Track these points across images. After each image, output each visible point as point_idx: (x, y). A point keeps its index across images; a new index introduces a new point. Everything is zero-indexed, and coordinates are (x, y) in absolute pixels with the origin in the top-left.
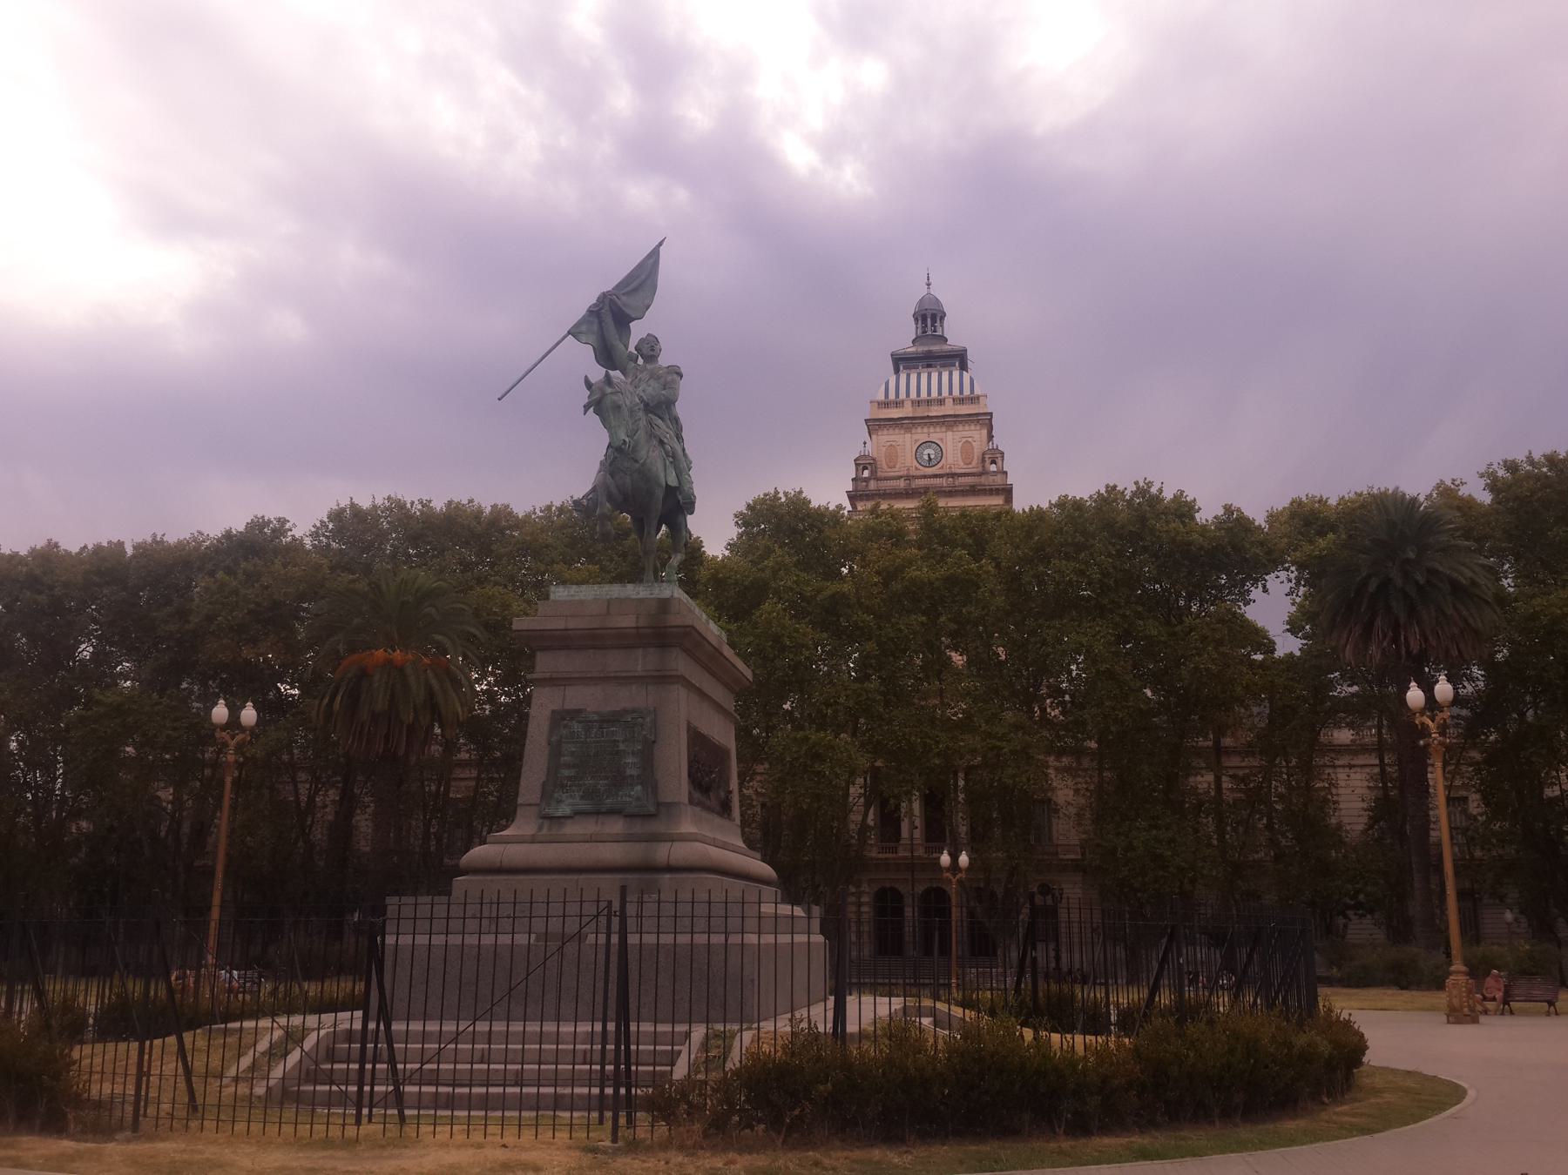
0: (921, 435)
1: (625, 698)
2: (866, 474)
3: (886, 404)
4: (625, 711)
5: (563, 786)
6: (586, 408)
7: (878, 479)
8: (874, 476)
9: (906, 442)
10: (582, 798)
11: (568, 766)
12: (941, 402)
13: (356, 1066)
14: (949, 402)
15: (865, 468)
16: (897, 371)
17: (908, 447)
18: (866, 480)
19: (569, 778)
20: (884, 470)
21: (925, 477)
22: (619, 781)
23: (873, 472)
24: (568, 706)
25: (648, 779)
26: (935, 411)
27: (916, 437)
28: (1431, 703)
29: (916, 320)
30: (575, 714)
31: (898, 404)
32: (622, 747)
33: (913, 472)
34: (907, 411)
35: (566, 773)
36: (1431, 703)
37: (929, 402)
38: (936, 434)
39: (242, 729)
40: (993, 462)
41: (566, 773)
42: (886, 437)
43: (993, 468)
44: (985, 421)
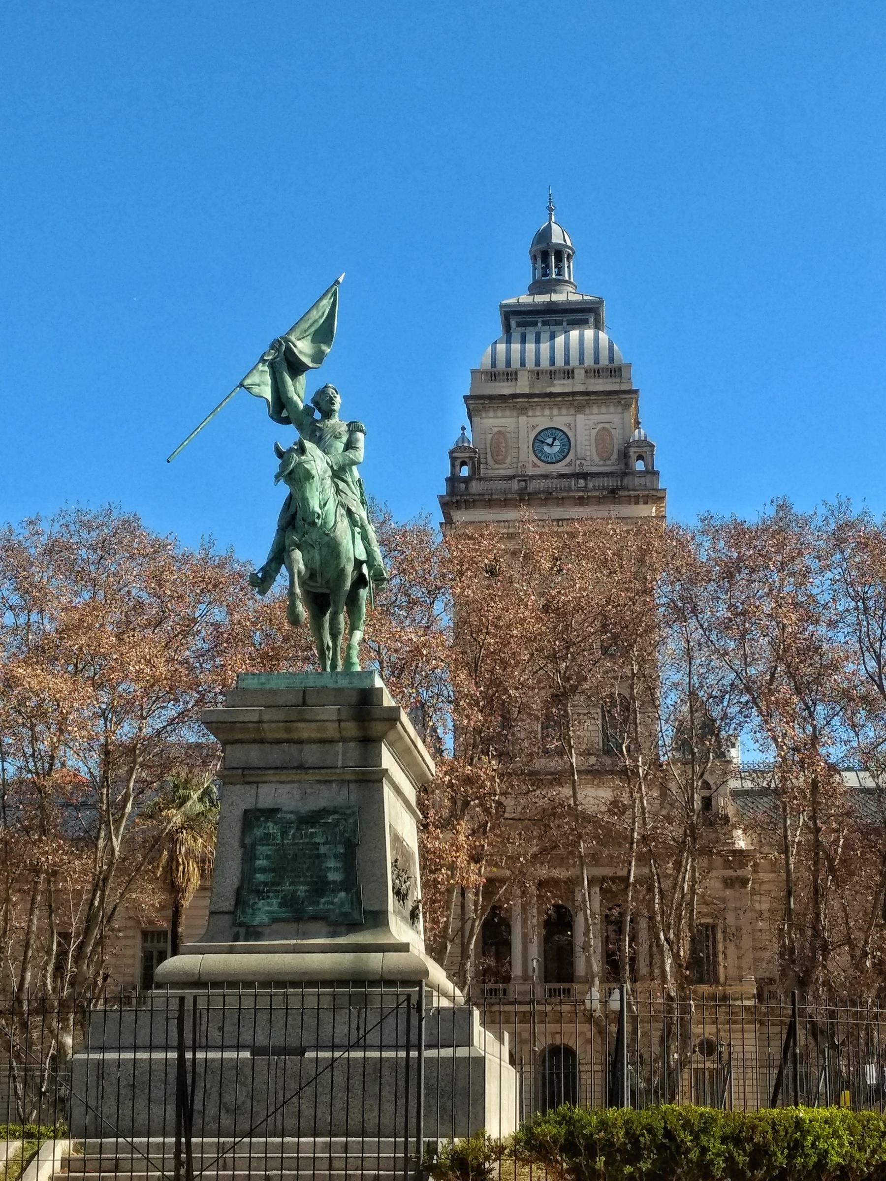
0: (542, 419)
2: (465, 471)
3: (493, 375)
4: (324, 812)
5: (259, 893)
6: (277, 477)
7: (481, 479)
8: (475, 473)
9: (524, 427)
10: (280, 905)
11: (263, 870)
12: (569, 374)
13: (174, 1140)
14: (580, 374)
15: (464, 463)
16: (507, 329)
17: (523, 433)
18: (467, 480)
19: (266, 884)
20: (492, 469)
21: (545, 476)
22: (320, 888)
23: (475, 470)
24: (261, 805)
26: (560, 386)
27: (533, 421)
29: (534, 258)
30: (271, 813)
31: (511, 376)
32: (323, 850)
33: (530, 471)
34: (523, 386)
35: (260, 877)
37: (552, 374)
38: (560, 419)
40: (640, 458)
41: (260, 877)
42: (495, 421)
43: (640, 466)
44: (624, 398)
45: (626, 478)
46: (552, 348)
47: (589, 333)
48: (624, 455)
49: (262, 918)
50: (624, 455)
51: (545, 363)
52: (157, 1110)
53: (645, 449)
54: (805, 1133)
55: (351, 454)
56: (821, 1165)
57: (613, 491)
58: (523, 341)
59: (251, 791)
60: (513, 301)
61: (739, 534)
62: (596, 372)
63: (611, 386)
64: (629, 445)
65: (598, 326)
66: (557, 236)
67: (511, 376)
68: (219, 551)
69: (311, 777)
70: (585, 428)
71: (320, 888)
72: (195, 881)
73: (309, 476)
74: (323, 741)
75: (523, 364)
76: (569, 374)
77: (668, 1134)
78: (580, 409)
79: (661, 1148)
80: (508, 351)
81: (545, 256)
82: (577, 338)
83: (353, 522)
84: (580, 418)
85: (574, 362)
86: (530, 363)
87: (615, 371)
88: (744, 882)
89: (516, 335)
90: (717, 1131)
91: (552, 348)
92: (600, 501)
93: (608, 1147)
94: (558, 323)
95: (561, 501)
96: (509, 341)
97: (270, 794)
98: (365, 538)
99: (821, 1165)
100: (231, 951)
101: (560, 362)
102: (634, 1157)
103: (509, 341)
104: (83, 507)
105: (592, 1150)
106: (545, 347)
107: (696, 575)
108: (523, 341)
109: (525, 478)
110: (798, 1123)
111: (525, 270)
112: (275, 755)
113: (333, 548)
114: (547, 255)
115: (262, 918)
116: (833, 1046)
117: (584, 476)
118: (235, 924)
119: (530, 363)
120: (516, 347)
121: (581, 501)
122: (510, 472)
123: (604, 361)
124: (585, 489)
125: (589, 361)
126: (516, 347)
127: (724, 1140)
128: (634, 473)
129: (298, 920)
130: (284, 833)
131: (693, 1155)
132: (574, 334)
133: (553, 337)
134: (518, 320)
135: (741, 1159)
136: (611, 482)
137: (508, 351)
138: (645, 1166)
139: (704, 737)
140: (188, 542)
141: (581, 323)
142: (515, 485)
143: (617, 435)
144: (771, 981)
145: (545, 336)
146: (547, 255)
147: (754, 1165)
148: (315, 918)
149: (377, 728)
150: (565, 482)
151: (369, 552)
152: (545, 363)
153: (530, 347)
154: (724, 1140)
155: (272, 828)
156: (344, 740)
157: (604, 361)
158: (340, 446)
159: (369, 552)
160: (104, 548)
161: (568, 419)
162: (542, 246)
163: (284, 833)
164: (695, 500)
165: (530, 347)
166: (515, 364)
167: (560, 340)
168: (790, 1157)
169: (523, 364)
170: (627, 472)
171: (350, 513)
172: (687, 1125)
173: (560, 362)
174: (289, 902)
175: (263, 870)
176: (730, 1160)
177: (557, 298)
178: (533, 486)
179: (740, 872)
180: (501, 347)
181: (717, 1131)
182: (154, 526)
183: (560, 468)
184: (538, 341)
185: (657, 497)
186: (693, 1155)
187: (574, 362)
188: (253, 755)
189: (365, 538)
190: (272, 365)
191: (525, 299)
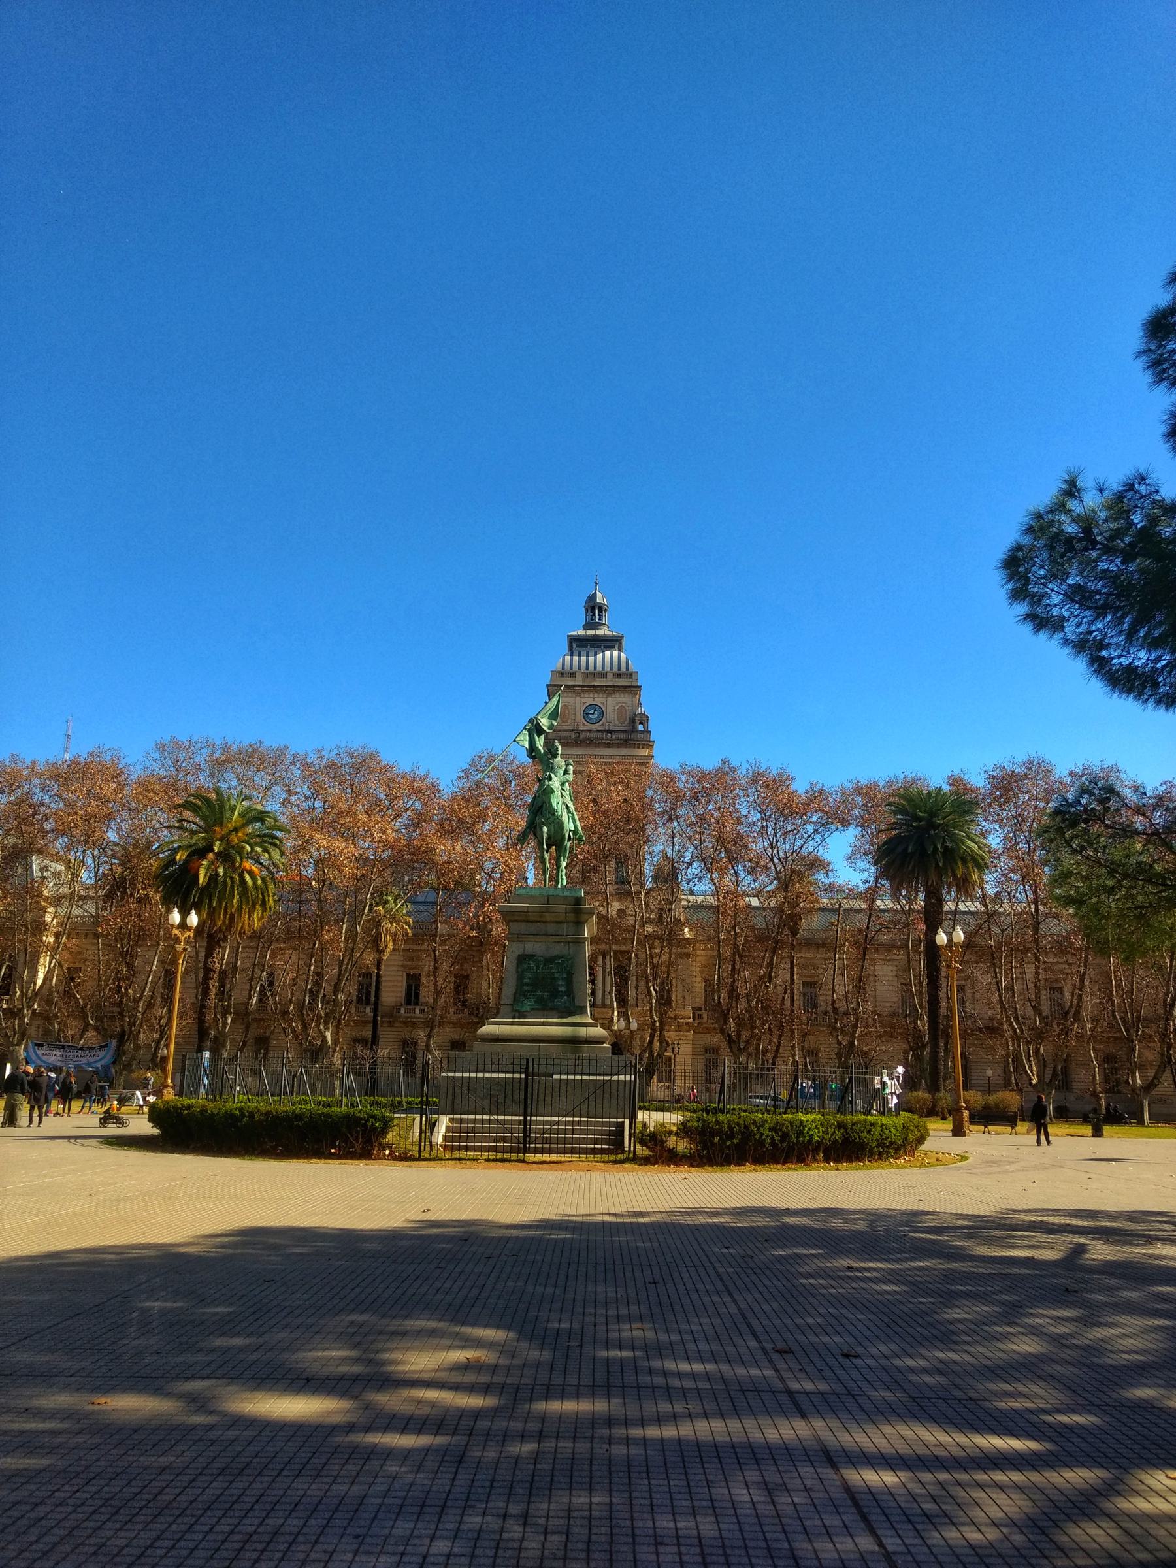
0: (588, 699)
1: (557, 950)
3: (563, 673)
4: (558, 957)
5: (525, 996)
11: (528, 984)
12: (604, 675)
14: (610, 676)
16: (571, 649)
22: (555, 994)
25: (570, 992)
27: (584, 700)
28: (183, 925)
29: (587, 610)
30: (531, 957)
31: (572, 674)
34: (579, 680)
35: (526, 988)
36: (183, 925)
38: (599, 700)
39: (189, 929)
41: (526, 988)
43: (641, 727)
44: (633, 690)
45: (632, 734)
46: (595, 660)
47: (615, 653)
48: (633, 721)
49: (526, 1008)
50: (633, 721)
51: (591, 668)
52: (480, 1103)
53: (644, 718)
54: (804, 1127)
55: (567, 777)
56: (810, 1141)
57: (626, 741)
58: (580, 655)
59: (521, 945)
60: (575, 633)
61: (703, 777)
62: (619, 675)
63: (626, 683)
64: (635, 716)
65: (620, 650)
66: (600, 599)
67: (572, 674)
68: (422, 772)
69: (551, 939)
70: (612, 705)
71: (555, 994)
72: (390, 945)
73: (553, 791)
74: (557, 922)
75: (579, 668)
76: (604, 675)
77: (746, 1127)
78: (609, 695)
79: (743, 1133)
80: (572, 660)
81: (593, 609)
82: (609, 656)
83: (569, 812)
84: (609, 699)
85: (607, 669)
86: (583, 668)
87: (630, 675)
88: (687, 955)
89: (576, 652)
90: (767, 1126)
91: (595, 660)
92: (619, 746)
93: (720, 1132)
94: (599, 647)
95: (597, 745)
96: (572, 655)
97: (532, 947)
98: (573, 819)
99: (810, 1141)
100: (512, 1024)
101: (599, 668)
102: (731, 1137)
103: (572, 655)
104: (349, 745)
105: (713, 1133)
106: (591, 659)
107: (679, 797)
108: (580, 655)
109: (578, 731)
110: (801, 1122)
111: (582, 617)
112: (532, 928)
113: (561, 825)
114: (593, 609)
115: (526, 1008)
116: (739, 1049)
117: (611, 732)
118: (513, 1010)
119: (583, 668)
120: (576, 658)
121: (609, 746)
122: (570, 728)
123: (623, 668)
124: (611, 739)
125: (615, 669)
126: (576, 658)
127: (770, 1130)
128: (638, 731)
129: (544, 1010)
130: (538, 967)
131: (757, 1137)
132: (608, 653)
133: (596, 655)
134: (577, 644)
135: (777, 1139)
136: (625, 736)
137: (572, 660)
138: (735, 1141)
139: (668, 876)
140: (405, 766)
141: (611, 647)
142: (573, 735)
143: (629, 709)
144: (700, 1009)
145: (592, 653)
146: (593, 609)
147: (782, 1141)
148: (552, 1009)
149: (584, 917)
150: (600, 735)
151: (575, 826)
152: (591, 668)
153: (584, 658)
154: (770, 1130)
155: (532, 965)
156: (568, 922)
157: (623, 668)
158: (562, 772)
159: (575, 826)
160: (357, 768)
161: (603, 700)
162: (591, 604)
163: (538, 967)
164: (675, 750)
165: (584, 658)
166: (575, 668)
167: (600, 656)
168: (797, 1138)
169: (579, 668)
170: (634, 730)
171: (567, 807)
172: (755, 1123)
173: (599, 668)
174: (540, 1000)
175: (528, 984)
176: (772, 1139)
177: (598, 633)
178: (583, 736)
179: (686, 950)
180: (568, 658)
181: (767, 1126)
182: (386, 757)
183: (598, 726)
184: (588, 655)
185: (649, 745)
186: (757, 1137)
187: (607, 669)
188: (523, 928)
189: (573, 819)
190: (529, 730)
191: (582, 632)
